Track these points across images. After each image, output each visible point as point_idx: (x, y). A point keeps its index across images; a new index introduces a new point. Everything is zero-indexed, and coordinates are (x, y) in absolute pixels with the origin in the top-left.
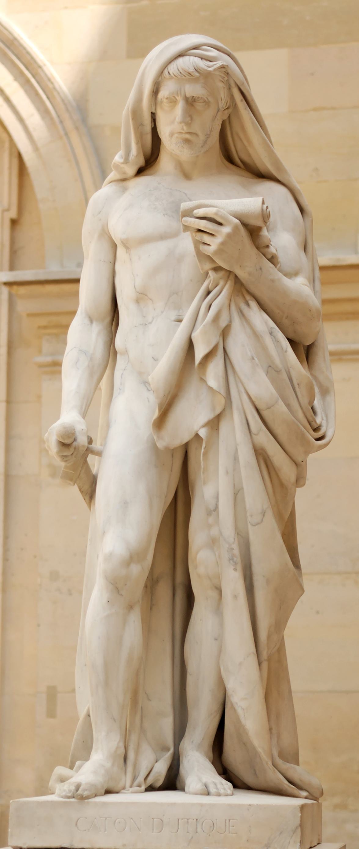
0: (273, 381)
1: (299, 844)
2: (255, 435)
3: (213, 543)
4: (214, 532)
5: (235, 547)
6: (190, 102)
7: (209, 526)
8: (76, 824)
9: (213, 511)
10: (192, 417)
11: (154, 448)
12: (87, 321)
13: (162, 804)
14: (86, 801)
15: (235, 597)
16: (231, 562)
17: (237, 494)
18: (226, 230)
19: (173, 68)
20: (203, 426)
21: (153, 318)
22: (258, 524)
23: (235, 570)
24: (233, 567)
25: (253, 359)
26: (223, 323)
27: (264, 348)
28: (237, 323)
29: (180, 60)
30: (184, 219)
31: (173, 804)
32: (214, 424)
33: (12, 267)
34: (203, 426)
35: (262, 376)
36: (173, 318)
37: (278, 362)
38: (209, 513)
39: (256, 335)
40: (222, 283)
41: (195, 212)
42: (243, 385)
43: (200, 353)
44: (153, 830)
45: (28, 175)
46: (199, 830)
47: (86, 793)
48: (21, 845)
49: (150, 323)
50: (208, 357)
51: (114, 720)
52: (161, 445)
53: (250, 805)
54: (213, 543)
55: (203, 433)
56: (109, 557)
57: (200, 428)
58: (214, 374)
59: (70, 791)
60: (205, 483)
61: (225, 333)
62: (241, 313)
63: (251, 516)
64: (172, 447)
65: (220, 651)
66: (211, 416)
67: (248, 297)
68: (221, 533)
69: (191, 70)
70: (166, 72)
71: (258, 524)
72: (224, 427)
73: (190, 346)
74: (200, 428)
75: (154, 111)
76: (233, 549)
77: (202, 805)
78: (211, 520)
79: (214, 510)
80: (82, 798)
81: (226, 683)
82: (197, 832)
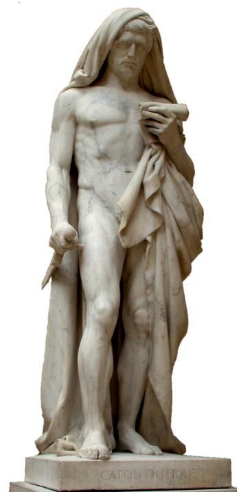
0: (187, 210)
3: (148, 305)
4: (150, 298)
6: (138, 45)
7: (147, 295)
8: (102, 476)
9: (150, 286)
10: (145, 227)
11: (118, 245)
12: (59, 168)
13: (153, 462)
15: (163, 337)
17: (165, 275)
19: (131, 25)
20: (150, 235)
26: (162, 176)
27: (181, 191)
30: (143, 112)
31: (160, 461)
32: (154, 234)
35: (182, 208)
36: (124, 170)
38: (147, 287)
40: (159, 152)
42: (172, 211)
43: (149, 192)
46: (175, 476)
48: (68, 489)
49: (109, 172)
52: (124, 245)
54: (148, 305)
55: (149, 239)
56: (101, 312)
58: (157, 206)
60: (147, 269)
61: (162, 181)
62: (170, 173)
67: (171, 162)
68: (156, 299)
69: (142, 27)
70: (126, 26)
71: (176, 295)
77: (175, 461)
78: (148, 291)
79: (151, 285)
81: (154, 388)
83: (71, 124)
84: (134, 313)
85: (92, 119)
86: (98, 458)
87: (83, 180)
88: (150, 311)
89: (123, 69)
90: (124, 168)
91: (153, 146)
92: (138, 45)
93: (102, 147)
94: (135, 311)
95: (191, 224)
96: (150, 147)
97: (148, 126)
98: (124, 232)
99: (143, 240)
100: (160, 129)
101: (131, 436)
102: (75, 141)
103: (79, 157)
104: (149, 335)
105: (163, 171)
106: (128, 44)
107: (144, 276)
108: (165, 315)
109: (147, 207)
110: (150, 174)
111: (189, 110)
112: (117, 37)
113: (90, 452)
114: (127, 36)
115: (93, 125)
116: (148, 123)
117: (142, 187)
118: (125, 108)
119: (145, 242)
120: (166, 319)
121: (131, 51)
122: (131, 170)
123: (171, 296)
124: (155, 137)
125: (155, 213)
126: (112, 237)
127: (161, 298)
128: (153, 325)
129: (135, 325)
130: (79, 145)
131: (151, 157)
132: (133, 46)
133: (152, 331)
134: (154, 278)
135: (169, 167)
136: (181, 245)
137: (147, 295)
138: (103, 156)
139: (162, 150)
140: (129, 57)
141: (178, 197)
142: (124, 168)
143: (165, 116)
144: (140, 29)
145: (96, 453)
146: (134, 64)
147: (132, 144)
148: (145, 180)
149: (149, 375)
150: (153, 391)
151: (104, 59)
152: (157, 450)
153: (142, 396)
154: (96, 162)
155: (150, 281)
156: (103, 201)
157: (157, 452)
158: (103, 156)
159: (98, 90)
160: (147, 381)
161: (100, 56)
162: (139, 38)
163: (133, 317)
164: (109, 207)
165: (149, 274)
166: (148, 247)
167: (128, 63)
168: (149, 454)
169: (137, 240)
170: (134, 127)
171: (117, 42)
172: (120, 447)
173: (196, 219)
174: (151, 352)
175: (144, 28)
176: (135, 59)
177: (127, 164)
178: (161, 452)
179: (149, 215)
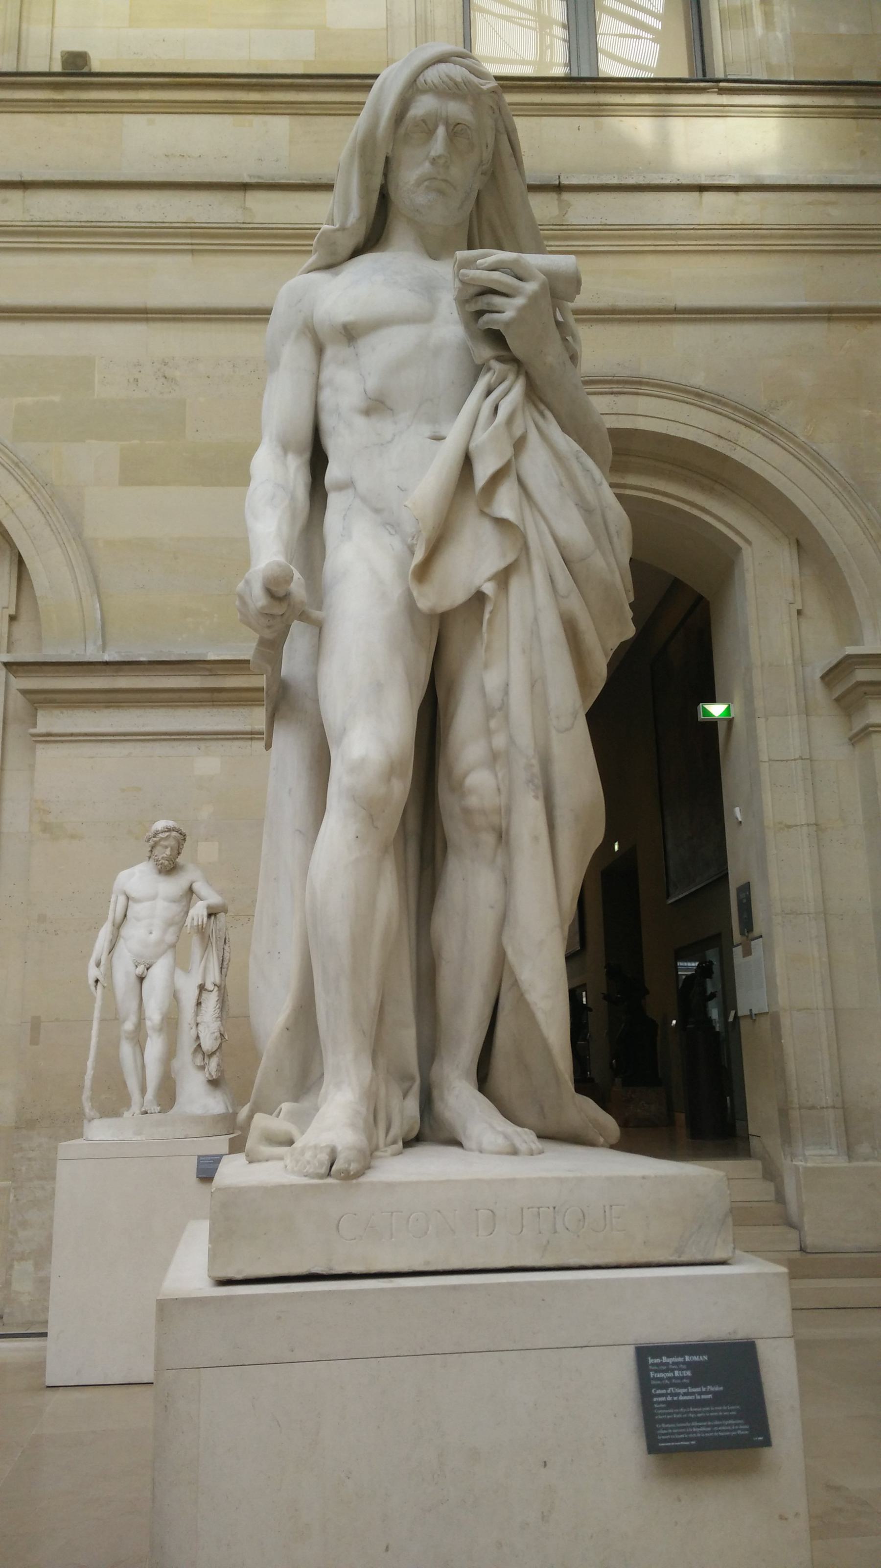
0: (587, 522)
1: (732, 1245)
2: (563, 597)
3: (494, 758)
4: (499, 741)
5: (535, 762)
6: (455, 130)
9: (496, 711)
10: (475, 559)
11: (410, 606)
12: (279, 450)
14: (354, 1181)
15: (536, 839)
16: (530, 785)
17: (536, 684)
18: (531, 287)
20: (489, 580)
21: (394, 435)
22: (567, 730)
23: (536, 797)
24: (533, 794)
25: (561, 485)
26: (518, 433)
28: (533, 437)
29: (442, 66)
32: (503, 577)
33: (8, 652)
34: (489, 580)
35: (575, 515)
36: (428, 434)
37: (590, 496)
38: (489, 713)
39: (557, 456)
40: (511, 377)
41: (479, 262)
43: (483, 473)
44: (478, 1230)
45: (27, 570)
47: (354, 1167)
50: (496, 478)
51: (364, 1033)
52: (424, 604)
53: (644, 1178)
54: (494, 758)
55: (489, 588)
57: (485, 582)
58: (506, 504)
59: (321, 1164)
60: (486, 666)
61: (519, 445)
63: (558, 718)
64: (440, 610)
65: (504, 920)
66: (502, 565)
68: (511, 741)
70: (421, 79)
71: (567, 730)
72: (516, 584)
73: (467, 463)
74: (485, 582)
75: (390, 154)
76: (532, 766)
78: (493, 724)
79: (500, 709)
80: (348, 1176)
82: (555, 1232)
83: (307, 349)
84: (461, 784)
85: (350, 318)
86: (329, 1174)
87: (333, 473)
88: (500, 775)
89: (421, 198)
90: (427, 430)
91: (496, 366)
92: (455, 130)
93: (372, 383)
94: (465, 775)
95: (598, 553)
96: (489, 369)
97: (480, 313)
98: (423, 572)
99: (473, 591)
100: (508, 310)
101: (461, 1098)
102: (317, 388)
103: (328, 422)
104: (502, 836)
105: (519, 421)
106: (427, 127)
107: (482, 688)
108: (538, 781)
109: (483, 513)
110: (485, 429)
111: (584, 279)
112: (400, 115)
113: (308, 1155)
114: (425, 105)
115: (350, 334)
116: (477, 300)
117: (467, 463)
118: (429, 289)
119: (479, 598)
120: (541, 794)
121: (439, 144)
122: (443, 434)
123: (554, 732)
124: (496, 338)
125: (501, 523)
126: (396, 592)
127: (525, 739)
128: (509, 811)
129: (467, 812)
130: (326, 396)
131: (489, 392)
132: (441, 131)
133: (314, 679)
134: (506, 689)
135: (541, 422)
136: (576, 605)
137: (489, 733)
138: (376, 406)
139: (517, 375)
140: (434, 161)
141: (561, 485)
142: (427, 430)
143: (521, 279)
144: (456, 84)
145: (324, 1157)
146: (445, 181)
147: (446, 371)
148: (472, 445)
149: (505, 940)
150: (516, 983)
151: (378, 181)
152: (525, 1138)
153: (493, 1002)
154: (360, 422)
155: (495, 698)
156: (377, 511)
157: (522, 1147)
158: (376, 406)
159: (366, 260)
160: (501, 963)
161: (366, 173)
162: (457, 109)
163: (458, 788)
164: (392, 525)
165: (492, 680)
166: (488, 608)
167: (432, 179)
168: (499, 1153)
169: (458, 596)
170: (449, 328)
171: (402, 131)
172: (430, 1129)
173: (611, 543)
174: (507, 881)
175: (467, 83)
176: (446, 167)
177: (433, 420)
178: (537, 1144)
179: (487, 529)
